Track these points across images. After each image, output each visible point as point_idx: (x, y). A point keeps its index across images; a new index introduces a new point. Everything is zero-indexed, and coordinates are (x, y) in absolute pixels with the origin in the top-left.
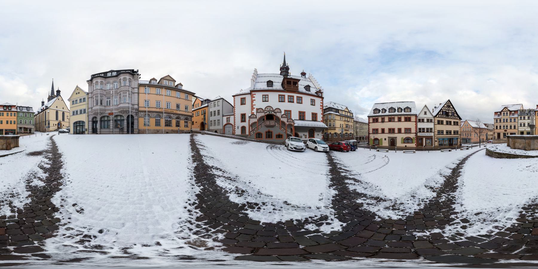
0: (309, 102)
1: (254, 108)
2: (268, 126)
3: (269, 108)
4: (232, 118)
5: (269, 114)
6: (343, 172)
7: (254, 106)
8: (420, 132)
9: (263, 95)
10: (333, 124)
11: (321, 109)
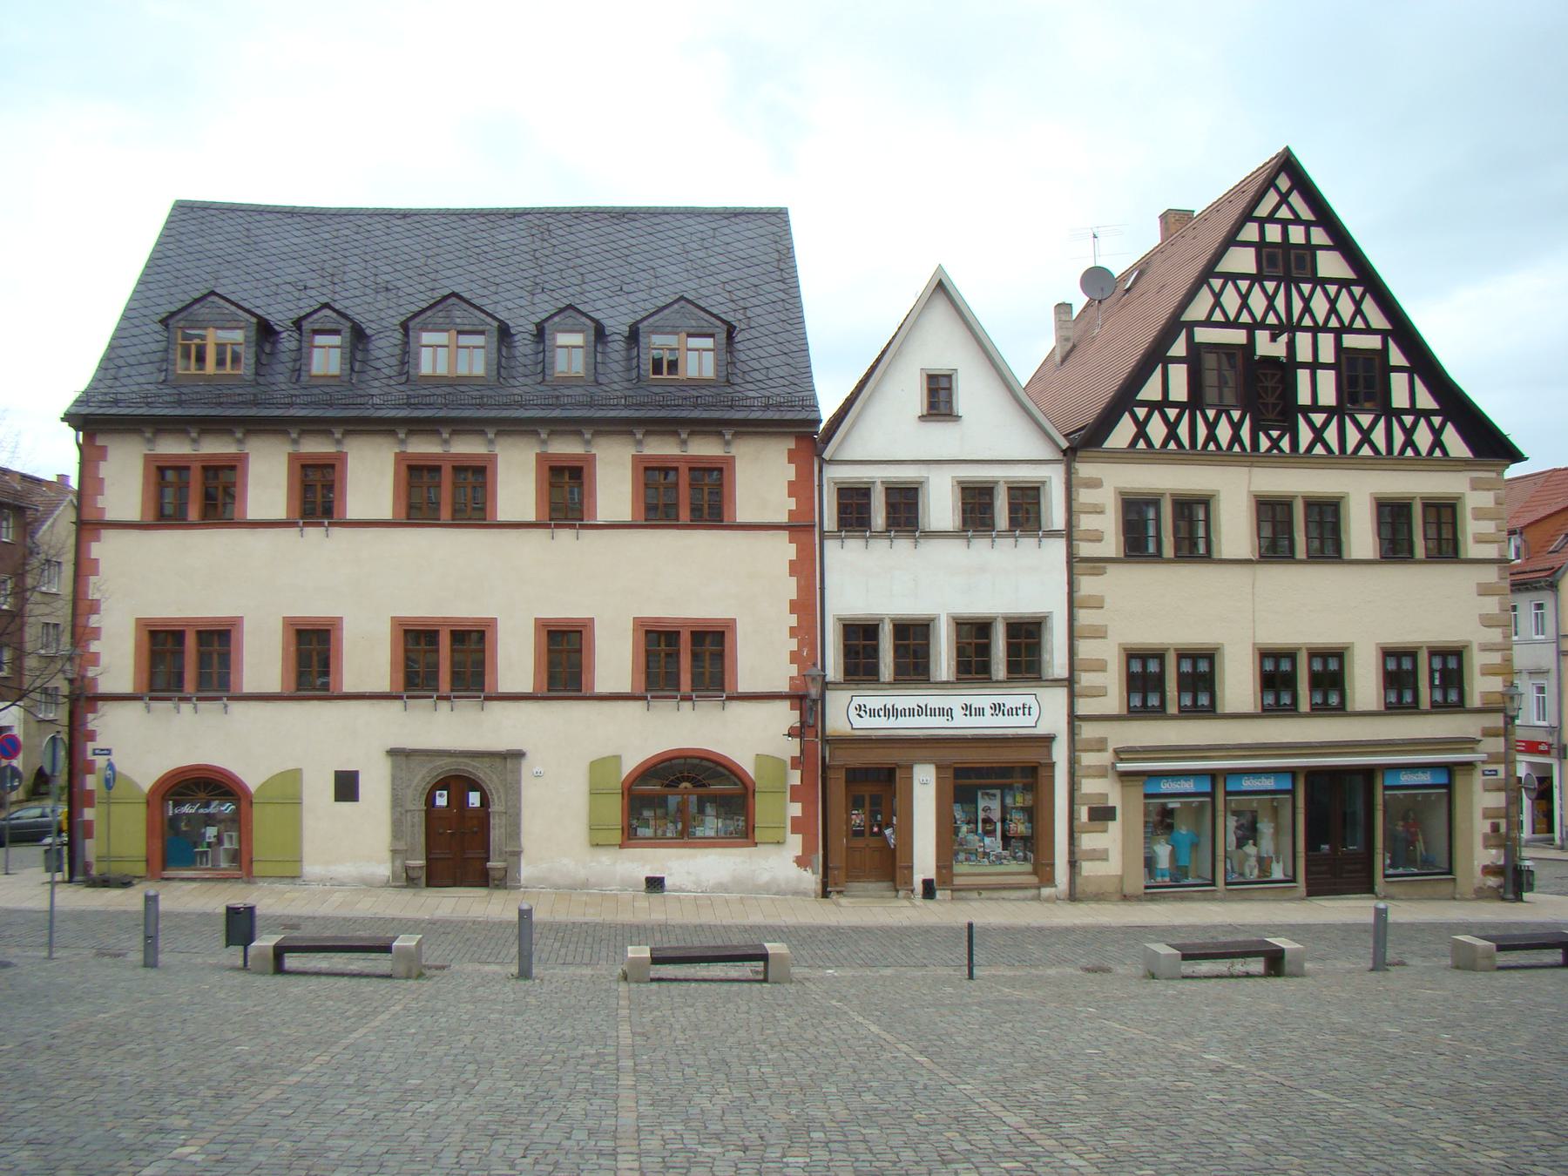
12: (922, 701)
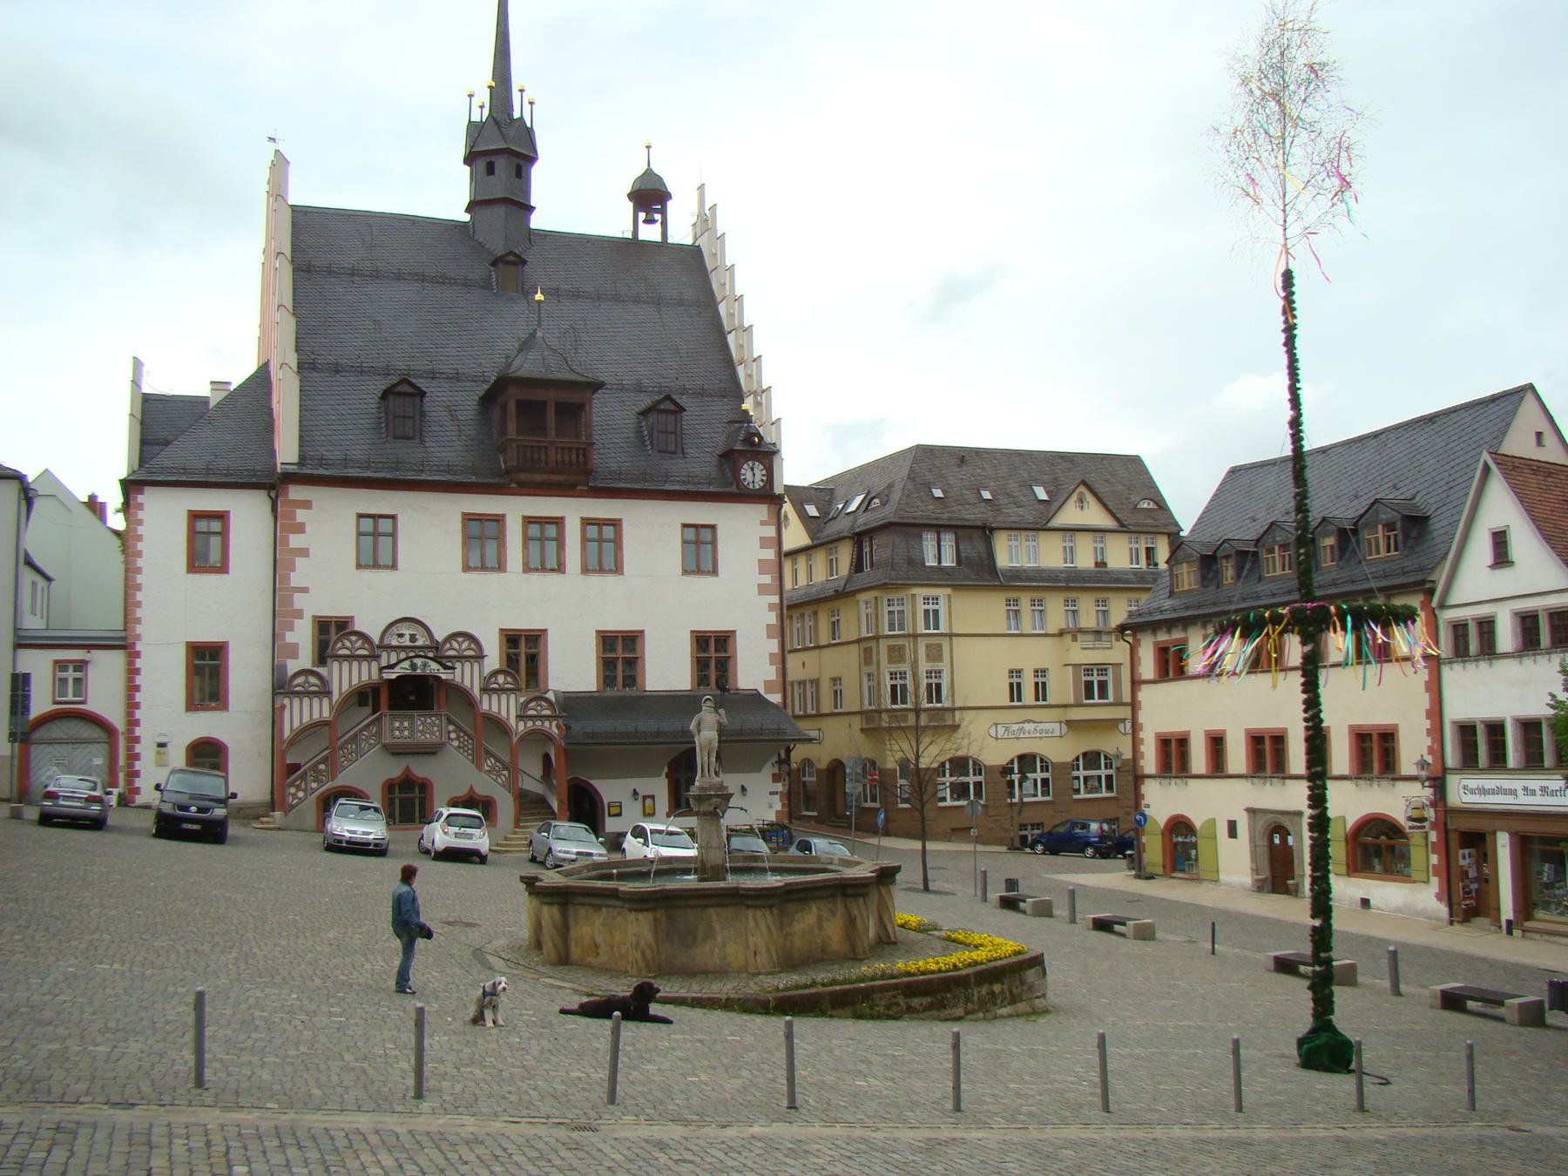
0: (672, 552)
1: (299, 614)
2: (396, 751)
3: (407, 632)
4: (105, 671)
5: (409, 672)
6: (1014, 1168)
7: (299, 601)
8: (1469, 761)
9: (360, 516)
10: (924, 682)
11: (763, 590)
12: (1499, 783)
